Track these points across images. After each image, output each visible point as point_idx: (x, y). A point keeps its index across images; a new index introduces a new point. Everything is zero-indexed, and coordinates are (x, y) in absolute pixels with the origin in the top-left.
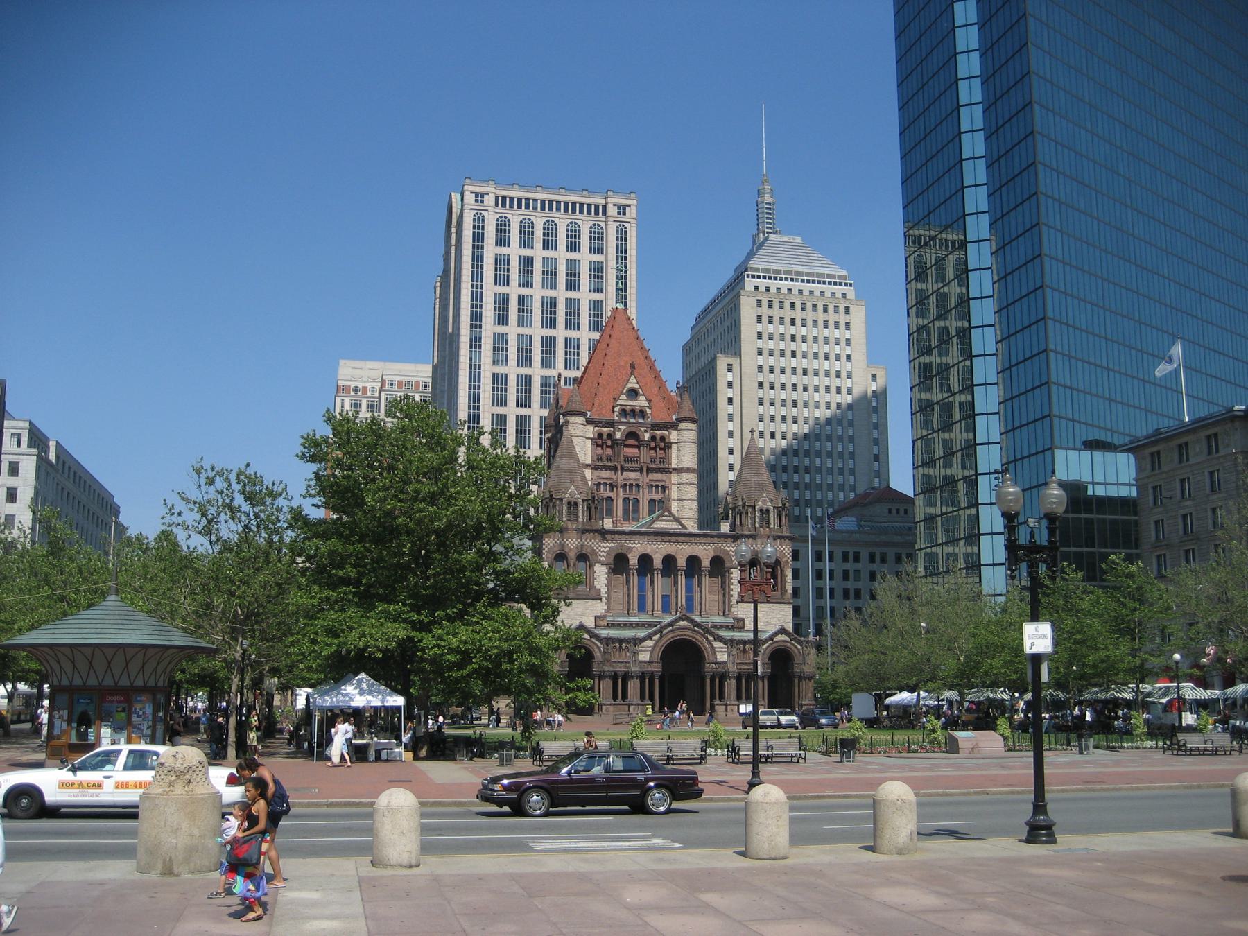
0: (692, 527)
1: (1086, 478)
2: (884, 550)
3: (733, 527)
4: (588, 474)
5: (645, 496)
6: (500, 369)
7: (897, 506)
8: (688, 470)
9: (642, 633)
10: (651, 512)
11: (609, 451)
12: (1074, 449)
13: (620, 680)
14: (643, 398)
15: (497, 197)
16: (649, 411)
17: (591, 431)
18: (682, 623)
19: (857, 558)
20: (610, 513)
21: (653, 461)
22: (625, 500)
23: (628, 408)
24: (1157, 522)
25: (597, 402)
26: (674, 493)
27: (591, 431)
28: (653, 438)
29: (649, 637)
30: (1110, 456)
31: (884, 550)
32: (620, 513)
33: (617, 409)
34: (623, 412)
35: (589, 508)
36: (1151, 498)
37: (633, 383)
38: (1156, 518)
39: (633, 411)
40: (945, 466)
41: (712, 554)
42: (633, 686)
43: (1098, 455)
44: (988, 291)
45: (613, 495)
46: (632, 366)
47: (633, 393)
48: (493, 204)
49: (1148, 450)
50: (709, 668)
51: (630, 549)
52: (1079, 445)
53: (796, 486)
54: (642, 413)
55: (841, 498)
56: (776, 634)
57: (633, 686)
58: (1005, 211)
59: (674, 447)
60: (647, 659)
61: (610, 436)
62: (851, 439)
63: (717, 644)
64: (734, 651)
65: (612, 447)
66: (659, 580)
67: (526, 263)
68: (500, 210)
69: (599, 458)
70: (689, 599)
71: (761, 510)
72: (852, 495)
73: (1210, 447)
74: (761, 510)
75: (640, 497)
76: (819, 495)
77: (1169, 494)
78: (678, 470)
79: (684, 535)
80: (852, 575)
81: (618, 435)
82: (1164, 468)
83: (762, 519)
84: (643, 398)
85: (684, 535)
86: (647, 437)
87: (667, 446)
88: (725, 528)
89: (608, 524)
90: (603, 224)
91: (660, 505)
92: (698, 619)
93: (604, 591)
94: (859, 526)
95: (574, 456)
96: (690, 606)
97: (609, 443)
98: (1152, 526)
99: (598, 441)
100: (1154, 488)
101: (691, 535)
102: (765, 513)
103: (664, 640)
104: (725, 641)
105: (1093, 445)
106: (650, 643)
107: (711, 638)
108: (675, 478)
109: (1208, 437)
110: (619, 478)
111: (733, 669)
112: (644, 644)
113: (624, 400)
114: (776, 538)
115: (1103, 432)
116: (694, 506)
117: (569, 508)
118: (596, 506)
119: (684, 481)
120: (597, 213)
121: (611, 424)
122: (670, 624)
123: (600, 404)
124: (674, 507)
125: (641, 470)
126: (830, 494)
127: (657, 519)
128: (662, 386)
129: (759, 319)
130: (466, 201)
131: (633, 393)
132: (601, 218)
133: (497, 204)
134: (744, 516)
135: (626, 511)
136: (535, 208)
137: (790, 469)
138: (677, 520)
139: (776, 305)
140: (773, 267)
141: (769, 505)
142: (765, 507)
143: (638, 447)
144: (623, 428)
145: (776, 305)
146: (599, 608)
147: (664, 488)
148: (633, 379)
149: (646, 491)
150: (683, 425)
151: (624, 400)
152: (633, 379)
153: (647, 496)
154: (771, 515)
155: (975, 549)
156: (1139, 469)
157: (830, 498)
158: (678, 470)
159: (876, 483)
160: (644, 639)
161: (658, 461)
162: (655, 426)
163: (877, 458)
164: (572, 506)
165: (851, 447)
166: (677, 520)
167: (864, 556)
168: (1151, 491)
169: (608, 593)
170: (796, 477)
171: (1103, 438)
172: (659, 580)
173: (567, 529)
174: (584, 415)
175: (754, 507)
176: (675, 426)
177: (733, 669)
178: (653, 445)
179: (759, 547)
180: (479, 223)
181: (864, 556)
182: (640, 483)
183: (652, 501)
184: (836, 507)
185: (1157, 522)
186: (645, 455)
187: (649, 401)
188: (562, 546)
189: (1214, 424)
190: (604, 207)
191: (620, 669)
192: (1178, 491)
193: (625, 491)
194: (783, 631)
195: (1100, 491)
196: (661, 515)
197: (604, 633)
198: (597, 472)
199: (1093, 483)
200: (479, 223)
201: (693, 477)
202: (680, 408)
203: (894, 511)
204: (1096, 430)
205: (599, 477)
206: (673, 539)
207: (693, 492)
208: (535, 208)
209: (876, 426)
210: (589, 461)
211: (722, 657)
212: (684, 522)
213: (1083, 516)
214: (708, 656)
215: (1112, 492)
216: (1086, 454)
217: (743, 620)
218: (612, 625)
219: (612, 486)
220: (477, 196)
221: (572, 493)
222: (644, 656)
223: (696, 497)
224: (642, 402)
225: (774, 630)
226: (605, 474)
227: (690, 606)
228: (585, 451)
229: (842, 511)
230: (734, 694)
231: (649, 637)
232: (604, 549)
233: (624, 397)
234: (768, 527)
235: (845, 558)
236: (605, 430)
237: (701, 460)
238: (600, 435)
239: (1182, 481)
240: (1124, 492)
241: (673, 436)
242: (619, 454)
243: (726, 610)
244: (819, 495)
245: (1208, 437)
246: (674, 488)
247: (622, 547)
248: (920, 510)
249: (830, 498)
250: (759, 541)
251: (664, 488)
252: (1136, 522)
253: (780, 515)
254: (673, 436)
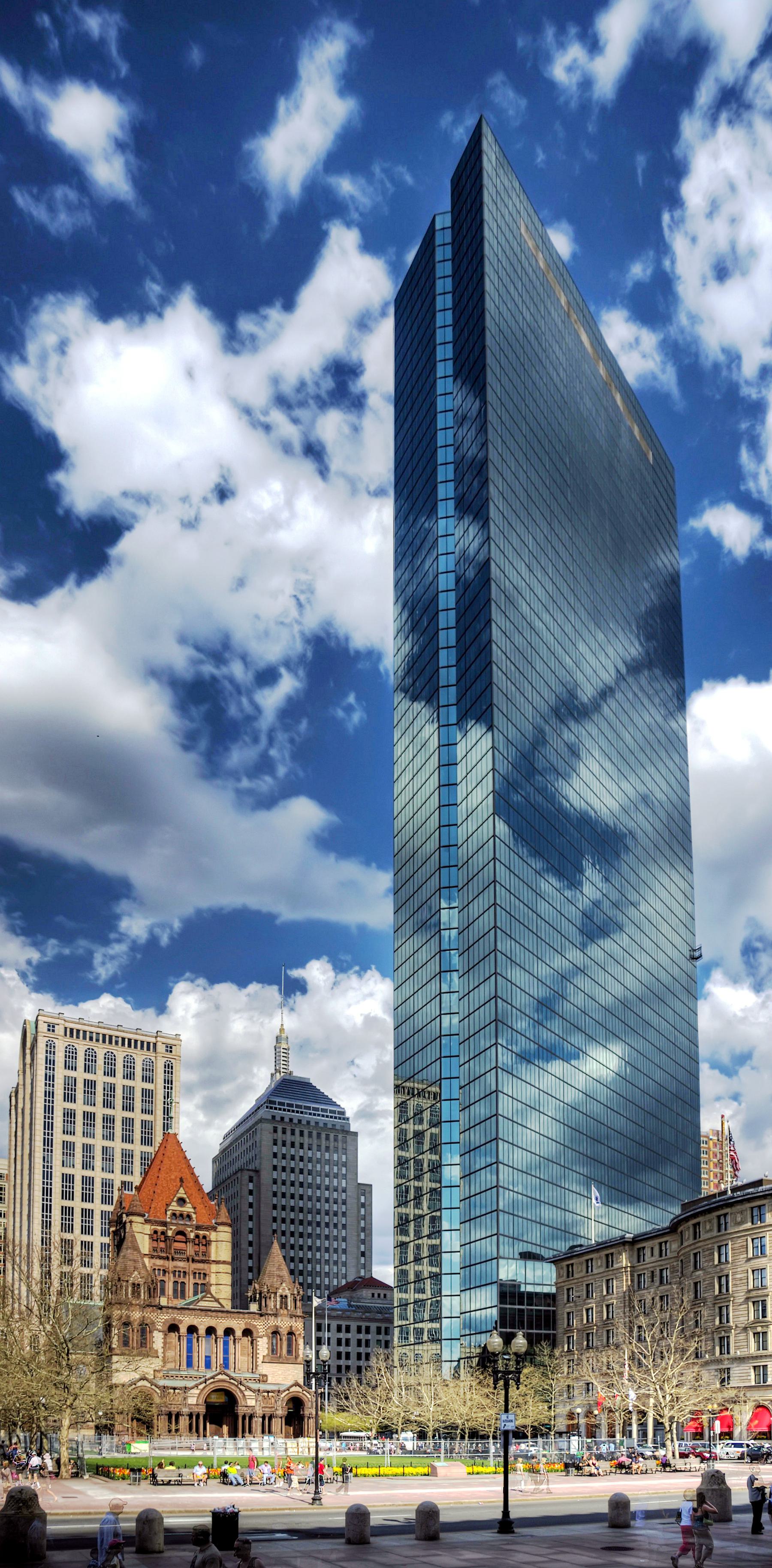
0: (228, 1305)
1: (520, 1279)
2: (368, 1324)
3: (260, 1308)
4: (146, 1260)
5: (190, 1282)
6: (68, 1171)
7: (379, 1291)
8: (224, 1262)
9: (190, 1384)
10: (196, 1293)
11: (162, 1245)
12: (513, 1259)
13: (173, 1417)
14: (189, 1205)
15: (66, 1028)
16: (194, 1216)
17: (148, 1229)
18: (220, 1377)
19: (348, 1330)
20: (163, 1292)
21: (197, 1253)
22: (176, 1282)
23: (178, 1213)
24: (568, 1314)
25: (153, 1206)
26: (213, 1279)
27: (148, 1229)
28: (197, 1236)
29: (197, 1386)
30: (538, 1264)
31: (368, 1324)
32: (171, 1292)
33: (169, 1213)
34: (174, 1214)
35: (149, 1290)
36: (566, 1296)
37: (182, 1193)
38: (568, 1310)
39: (181, 1215)
40: (407, 1215)
41: (243, 1327)
42: (184, 1422)
43: (530, 1264)
44: (456, 1204)
45: (166, 1279)
46: (181, 1180)
47: (182, 1201)
48: (62, 1033)
49: (565, 1261)
50: (241, 1411)
51: (181, 1321)
52: (517, 1256)
53: (292, 1247)
54: (189, 1216)
55: (335, 1283)
56: (291, 1386)
57: (184, 1422)
58: (472, 1033)
59: (213, 1244)
60: (195, 1403)
61: (163, 1233)
62: (344, 1239)
63: (248, 1393)
64: (260, 1398)
65: (165, 1241)
66: (203, 1342)
67: (90, 1085)
68: (68, 1039)
69: (155, 1249)
70: (226, 1360)
71: (281, 1296)
72: (344, 1282)
73: (608, 1262)
74: (281, 1296)
75: (186, 1281)
76: (318, 1281)
77: (578, 1294)
78: (217, 1262)
79: (222, 1312)
80: (343, 1342)
81: (170, 1233)
82: (576, 1276)
83: (281, 1302)
84: (189, 1205)
85: (222, 1312)
86: (192, 1236)
87: (208, 1243)
88: (254, 1307)
89: (164, 1301)
90: (153, 1059)
91: (203, 1288)
92: (233, 1375)
93: (160, 1351)
94: (349, 1305)
95: (136, 1249)
96: (226, 1364)
97: (163, 1239)
98: (565, 1316)
99: (154, 1236)
100: (568, 1290)
101: (228, 1312)
102: (284, 1298)
103: (207, 1389)
104: (254, 1391)
105: (527, 1256)
106: (196, 1391)
107: (243, 1388)
108: (214, 1268)
109: (607, 1256)
110: (170, 1265)
111: (259, 1412)
112: (192, 1391)
113: (174, 1207)
114: (292, 1316)
115: (534, 1246)
116: (228, 1290)
117: (133, 1288)
118: (154, 1288)
119: (221, 1270)
120: (148, 1049)
121: (164, 1224)
122: (213, 1378)
123: (155, 1208)
124: (213, 1289)
125: (188, 1260)
126: (327, 1280)
127: (202, 1299)
128: (200, 1188)
129: (275, 1143)
130: (39, 1029)
131: (182, 1201)
132: (151, 1054)
133: (66, 1035)
134: (268, 1300)
135: (175, 1291)
136: (97, 1040)
137: (297, 1260)
138: (217, 1300)
139: (289, 1132)
140: (287, 1101)
141: (287, 1293)
142: (284, 1294)
143: (186, 1243)
144: (174, 1228)
145: (289, 1132)
146: (157, 1363)
147: (205, 1275)
148: (182, 1191)
149: (191, 1277)
150: (220, 1228)
151: (174, 1207)
152: (182, 1191)
153: (192, 1281)
154: (289, 1300)
155: (438, 1325)
156: (559, 1276)
157: (327, 1283)
158: (217, 1262)
159: (362, 1273)
160: (193, 1388)
161: (200, 1254)
162: (198, 1228)
163: (363, 1254)
164: (136, 1286)
165: (344, 1246)
166: (217, 1300)
167: (354, 1328)
168: (565, 1292)
169: (164, 1353)
170: (301, 1266)
171: (534, 1251)
172: (203, 1342)
173: (131, 1304)
174: (143, 1216)
175: (276, 1293)
176: (214, 1229)
177: (259, 1412)
178: (197, 1242)
179: (279, 1324)
180: (51, 1049)
181: (354, 1328)
182: (187, 1271)
183: (196, 1284)
184: (332, 1290)
185: (568, 1314)
186: (190, 1250)
187: (195, 1208)
188: (128, 1317)
189: (611, 1246)
190: (155, 1044)
191: (174, 1409)
192: (585, 1292)
193: (175, 1275)
194: (297, 1384)
195: (530, 1289)
196: (204, 1297)
197: (162, 1383)
198: (153, 1261)
199: (526, 1284)
200: (51, 1049)
201: (228, 1268)
202: (218, 1215)
203: (376, 1295)
204: (530, 1245)
205: (154, 1264)
206: (214, 1314)
207: (227, 1279)
208: (97, 1040)
209: (363, 1230)
210: (147, 1253)
211: (251, 1402)
212: (221, 1301)
213: (517, 1307)
214: (241, 1402)
215: (538, 1289)
216: (522, 1262)
217: (266, 1376)
218: (166, 1377)
219: (164, 1271)
220: (49, 1026)
221: (135, 1277)
222: (192, 1401)
223: (229, 1283)
224: (188, 1209)
225: (290, 1383)
226: (159, 1262)
227: (226, 1364)
228: (145, 1244)
229: (337, 1292)
230: (259, 1429)
231: (197, 1386)
232: (161, 1319)
233: (174, 1204)
234: (286, 1308)
235: (339, 1329)
236: (160, 1228)
237: (233, 1258)
238: (156, 1232)
239: (588, 1285)
240: (546, 1290)
241: (213, 1236)
242: (170, 1248)
243: (254, 1368)
244: (318, 1281)
245: (607, 1256)
246: (213, 1276)
247: (174, 1319)
248: (397, 1295)
249: (327, 1283)
250: (279, 1319)
251: (205, 1275)
252: (554, 1312)
253: (295, 1301)
254: (213, 1236)
